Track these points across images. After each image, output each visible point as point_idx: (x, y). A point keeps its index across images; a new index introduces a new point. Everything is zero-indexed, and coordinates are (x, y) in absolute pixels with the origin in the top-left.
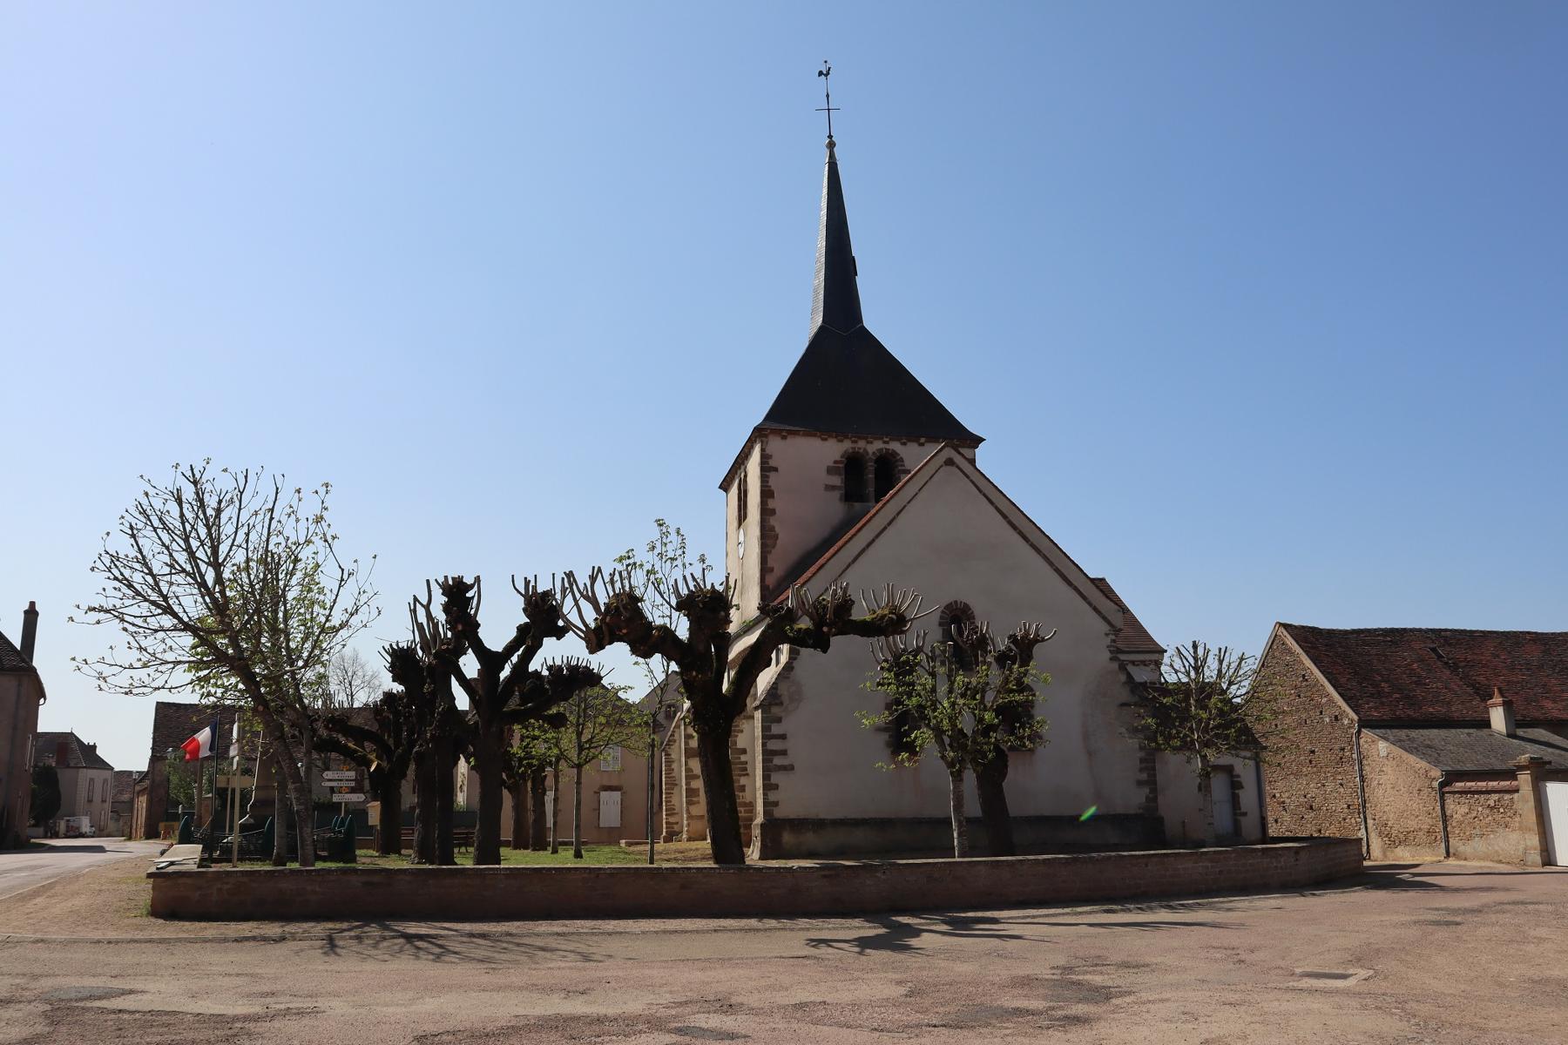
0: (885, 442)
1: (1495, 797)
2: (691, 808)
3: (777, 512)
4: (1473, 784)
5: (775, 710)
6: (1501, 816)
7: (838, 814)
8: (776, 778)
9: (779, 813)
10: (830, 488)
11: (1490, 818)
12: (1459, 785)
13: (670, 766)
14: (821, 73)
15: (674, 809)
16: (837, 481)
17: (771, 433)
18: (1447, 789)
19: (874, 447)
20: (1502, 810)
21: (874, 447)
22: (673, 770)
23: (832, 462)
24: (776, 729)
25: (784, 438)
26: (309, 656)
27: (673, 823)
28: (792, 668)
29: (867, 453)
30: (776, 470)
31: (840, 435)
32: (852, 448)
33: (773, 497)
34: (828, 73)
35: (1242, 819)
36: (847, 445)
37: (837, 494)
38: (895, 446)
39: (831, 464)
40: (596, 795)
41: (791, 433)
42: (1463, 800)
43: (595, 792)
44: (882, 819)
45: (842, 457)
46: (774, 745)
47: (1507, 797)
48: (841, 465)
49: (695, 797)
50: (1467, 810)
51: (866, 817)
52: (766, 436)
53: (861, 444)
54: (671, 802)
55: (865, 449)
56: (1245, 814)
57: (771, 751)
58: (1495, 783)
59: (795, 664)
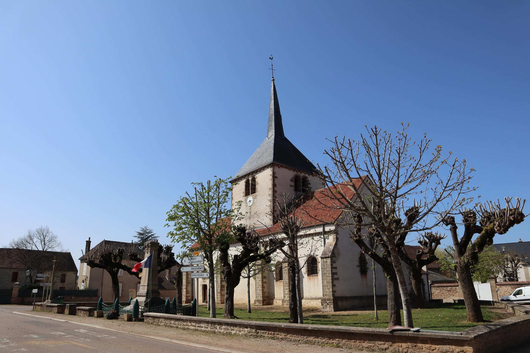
0: (305, 174)
1: (450, 288)
2: (222, 292)
3: (277, 192)
4: (441, 284)
5: (334, 258)
6: (452, 293)
7: (350, 295)
8: (335, 282)
9: (337, 294)
10: (291, 186)
11: (448, 293)
12: (436, 285)
13: (188, 276)
14: (270, 58)
15: (189, 291)
16: (293, 184)
17: (276, 165)
18: (432, 286)
19: (302, 175)
20: (452, 291)
21: (302, 175)
22: (189, 278)
23: (291, 177)
24: (334, 265)
25: (279, 167)
26: (318, 226)
27: (188, 296)
28: (337, 244)
29: (300, 176)
30: (277, 178)
31: (294, 170)
32: (297, 174)
33: (276, 186)
34: (272, 59)
35: (426, 294)
36: (295, 173)
37: (293, 188)
38: (307, 175)
39: (291, 178)
40: (136, 285)
41: (282, 166)
42: (438, 288)
43: (136, 284)
44: (360, 296)
45: (294, 176)
46: (334, 271)
47: (454, 288)
48: (294, 179)
49: (223, 288)
50: (439, 291)
51: (356, 296)
52: (274, 166)
53: (299, 173)
54: (188, 289)
55: (300, 175)
56: (426, 293)
57: (333, 273)
58: (449, 284)
59: (338, 243)
